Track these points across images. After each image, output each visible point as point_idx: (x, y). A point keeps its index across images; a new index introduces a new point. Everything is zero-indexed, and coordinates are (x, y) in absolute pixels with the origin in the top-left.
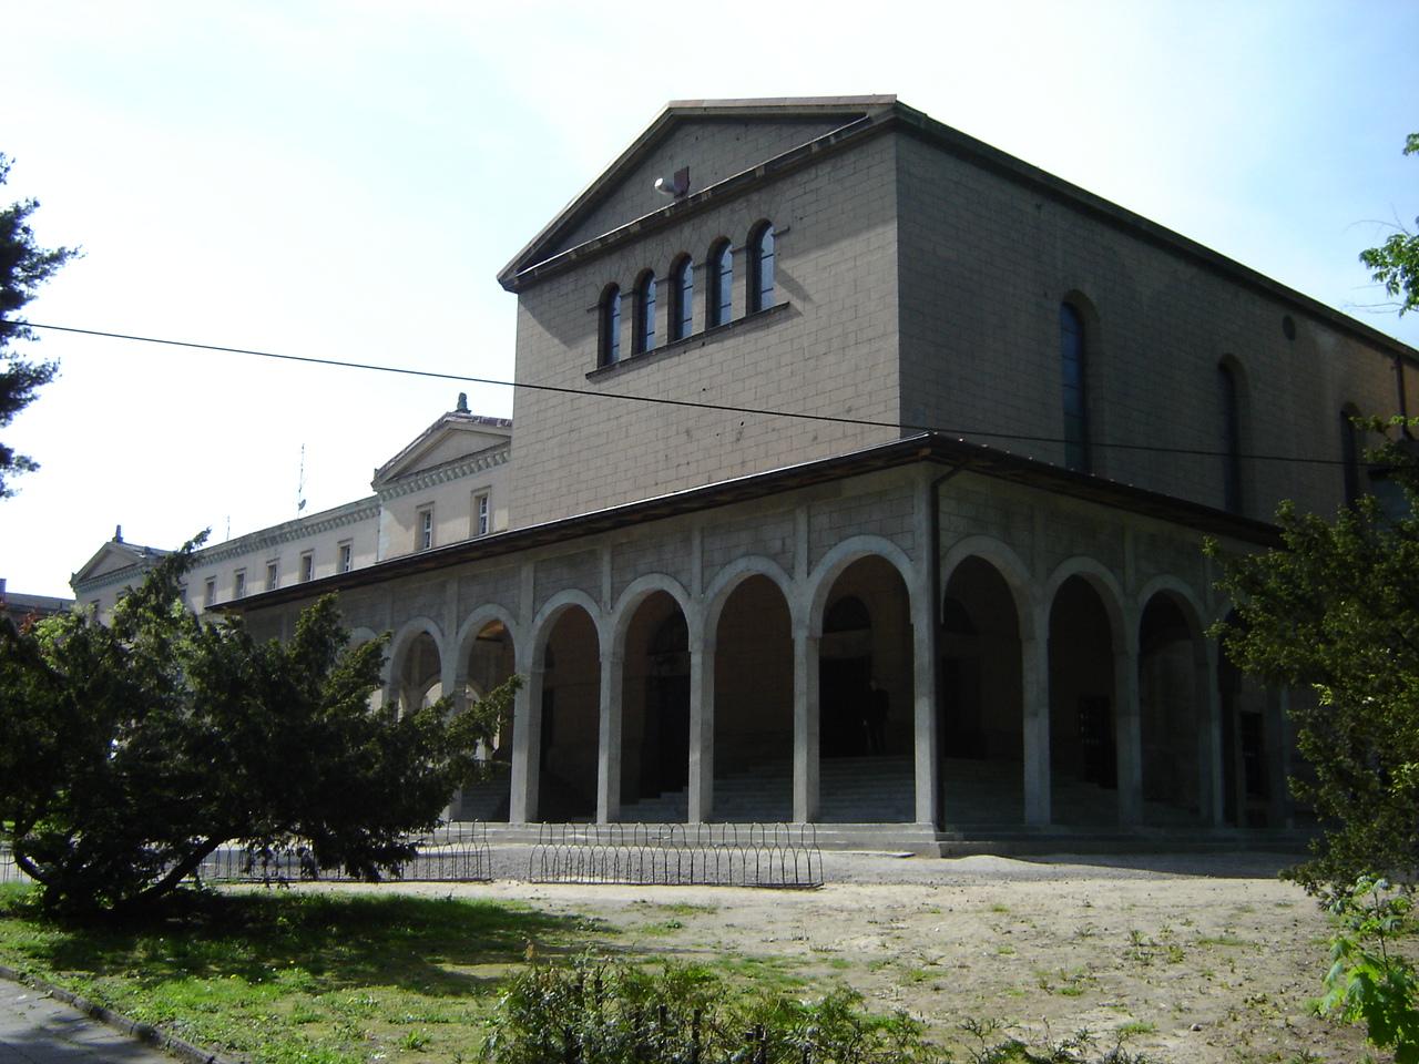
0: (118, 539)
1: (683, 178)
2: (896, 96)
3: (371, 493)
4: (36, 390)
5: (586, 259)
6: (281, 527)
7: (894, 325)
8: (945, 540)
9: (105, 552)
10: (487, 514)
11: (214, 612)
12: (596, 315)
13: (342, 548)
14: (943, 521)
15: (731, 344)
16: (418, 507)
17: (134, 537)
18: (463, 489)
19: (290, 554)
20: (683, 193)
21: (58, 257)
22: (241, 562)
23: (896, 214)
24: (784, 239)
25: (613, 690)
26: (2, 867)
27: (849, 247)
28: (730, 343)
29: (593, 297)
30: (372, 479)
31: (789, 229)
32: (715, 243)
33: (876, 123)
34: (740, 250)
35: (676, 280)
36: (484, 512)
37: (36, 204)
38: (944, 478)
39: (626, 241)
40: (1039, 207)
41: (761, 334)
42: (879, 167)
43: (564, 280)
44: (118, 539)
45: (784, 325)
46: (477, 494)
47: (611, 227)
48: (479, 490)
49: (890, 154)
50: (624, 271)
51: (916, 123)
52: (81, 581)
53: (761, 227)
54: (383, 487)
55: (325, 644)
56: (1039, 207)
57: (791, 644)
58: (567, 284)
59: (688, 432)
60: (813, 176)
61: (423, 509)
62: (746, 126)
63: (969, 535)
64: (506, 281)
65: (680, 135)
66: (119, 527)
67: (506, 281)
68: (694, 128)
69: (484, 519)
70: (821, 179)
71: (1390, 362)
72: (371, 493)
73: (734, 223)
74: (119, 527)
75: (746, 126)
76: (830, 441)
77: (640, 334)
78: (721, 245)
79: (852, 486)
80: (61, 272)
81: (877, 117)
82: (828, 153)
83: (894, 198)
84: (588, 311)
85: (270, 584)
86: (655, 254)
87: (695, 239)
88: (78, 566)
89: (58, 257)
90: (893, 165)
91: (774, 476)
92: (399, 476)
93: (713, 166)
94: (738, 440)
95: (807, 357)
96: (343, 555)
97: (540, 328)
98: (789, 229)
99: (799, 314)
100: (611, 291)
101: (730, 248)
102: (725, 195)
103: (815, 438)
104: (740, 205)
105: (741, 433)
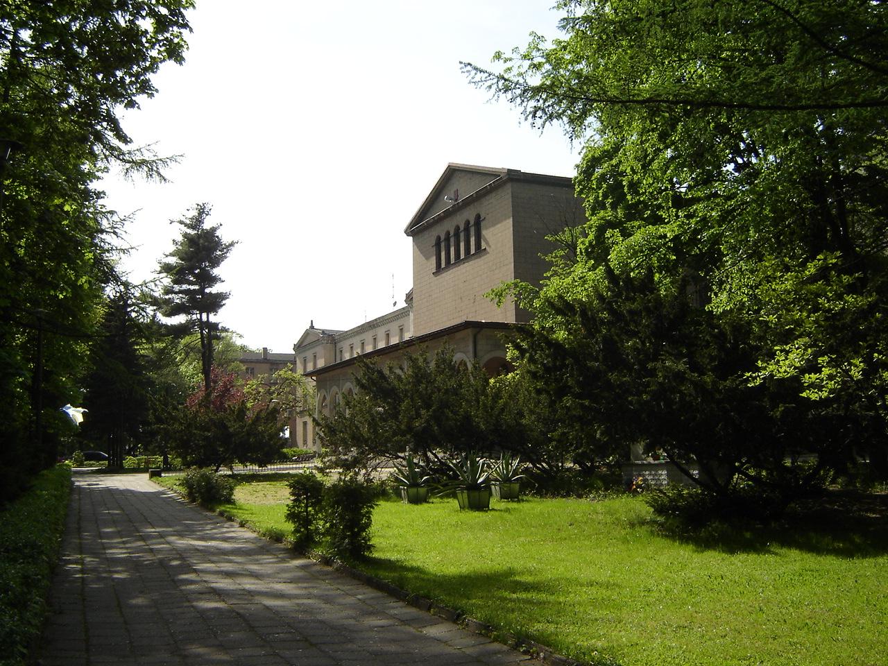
0: (312, 327)
4: (224, 302)
6: (376, 320)
8: (480, 354)
9: (307, 334)
14: (479, 347)
17: (320, 325)
19: (381, 332)
20: (456, 200)
21: (232, 244)
22: (363, 336)
27: (504, 223)
28: (444, 275)
37: (221, 225)
38: (478, 332)
39: (440, 220)
41: (479, 260)
42: (503, 201)
44: (312, 327)
45: (485, 257)
47: (438, 212)
49: (509, 191)
52: (298, 347)
55: (243, 410)
63: (492, 351)
66: (312, 321)
74: (312, 321)
79: (459, 335)
80: (234, 250)
85: (375, 347)
89: (232, 244)
93: (467, 189)
97: (419, 252)
99: (488, 253)
100: (439, 238)
102: (468, 202)
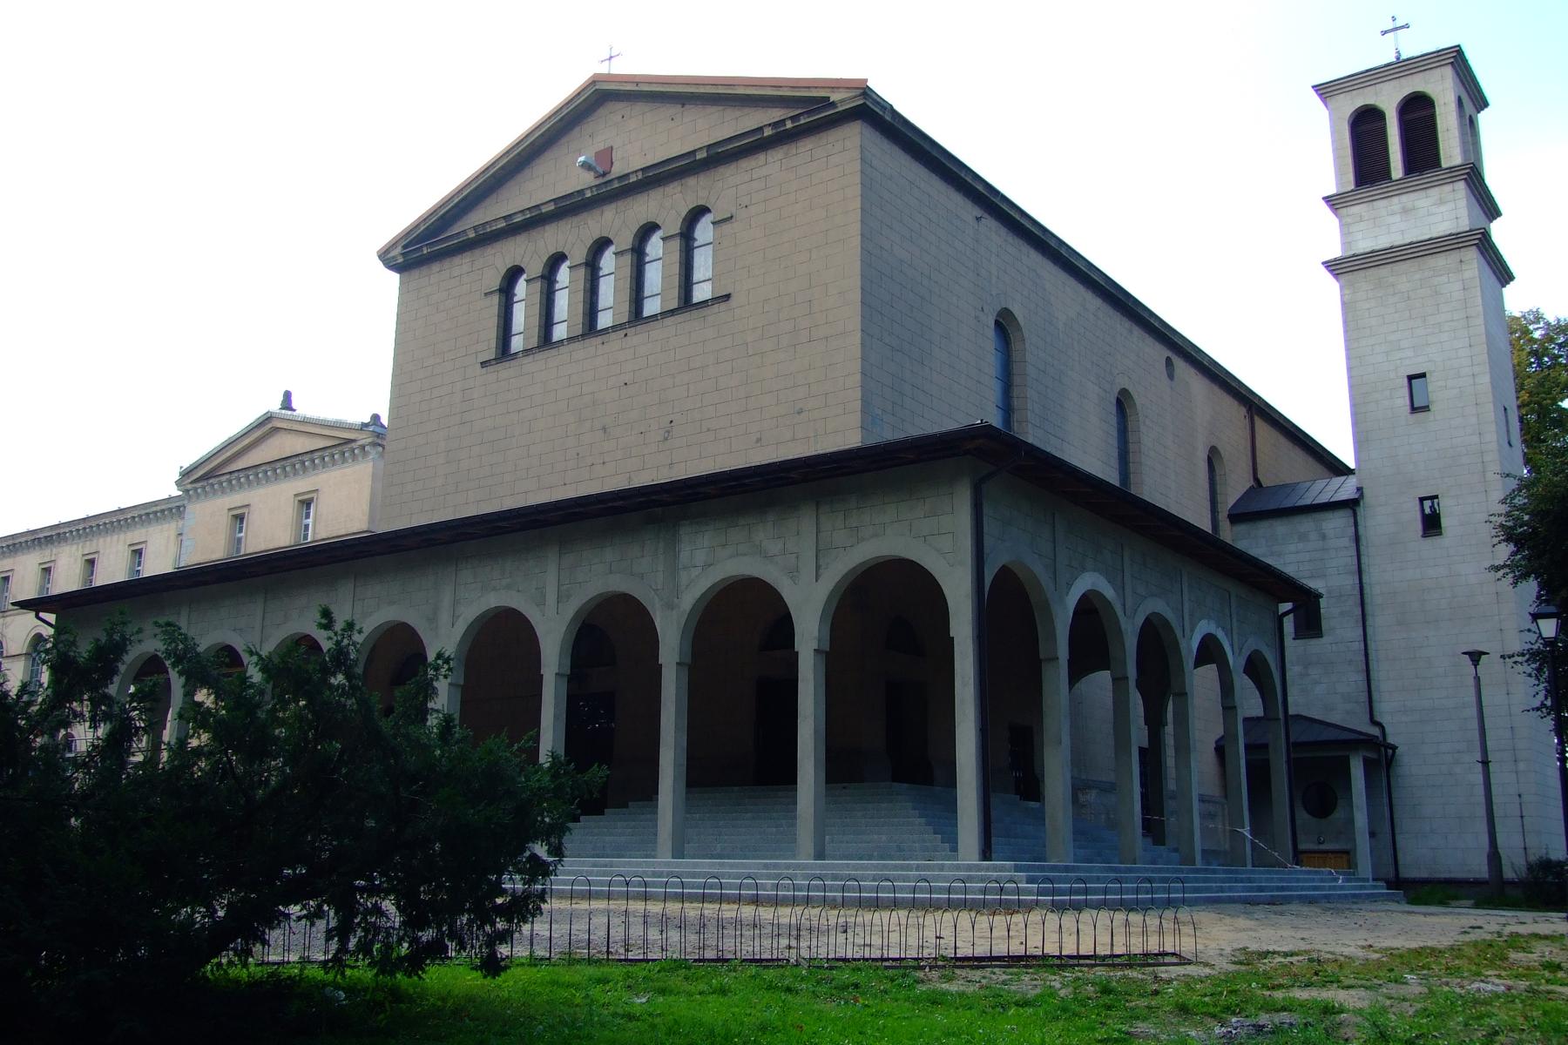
1: (607, 155)
2: (866, 80)
3: (175, 492)
5: (487, 238)
7: (855, 323)
10: (310, 521)
11: (22, 608)
12: (496, 299)
13: (133, 551)
15: (658, 331)
16: (230, 510)
17: (305, 407)
18: (283, 493)
22: (136, 535)
23: (859, 206)
24: (726, 227)
25: (556, 706)
26: (1396, 1044)
29: (495, 281)
30: (177, 478)
31: (732, 217)
32: (596, 242)
33: (840, 109)
34: (672, 236)
35: (548, 278)
36: (241, 531)
39: (535, 220)
40: (978, 219)
43: (457, 260)
46: (300, 498)
48: (304, 493)
49: (856, 140)
50: (530, 251)
51: (881, 113)
53: (698, 213)
54: (189, 487)
56: (978, 219)
57: (658, 670)
58: (461, 265)
59: (604, 429)
60: (761, 163)
61: (235, 512)
62: (683, 105)
64: (386, 257)
65: (602, 111)
67: (386, 257)
68: (619, 105)
69: (307, 527)
70: (771, 164)
71: (1243, 411)
72: (176, 492)
73: (668, 205)
75: (683, 105)
76: (777, 444)
77: (547, 322)
78: (557, 260)
81: (842, 101)
82: (782, 137)
83: (858, 190)
84: (486, 294)
86: (573, 237)
87: (619, 221)
88: (189, 460)
90: (857, 154)
91: (317, 549)
92: (205, 477)
94: (666, 439)
95: (750, 353)
96: (43, 578)
98: (732, 217)
100: (514, 273)
101: (524, 276)
102: (657, 177)
103: (759, 440)
104: (674, 189)
105: (668, 432)
